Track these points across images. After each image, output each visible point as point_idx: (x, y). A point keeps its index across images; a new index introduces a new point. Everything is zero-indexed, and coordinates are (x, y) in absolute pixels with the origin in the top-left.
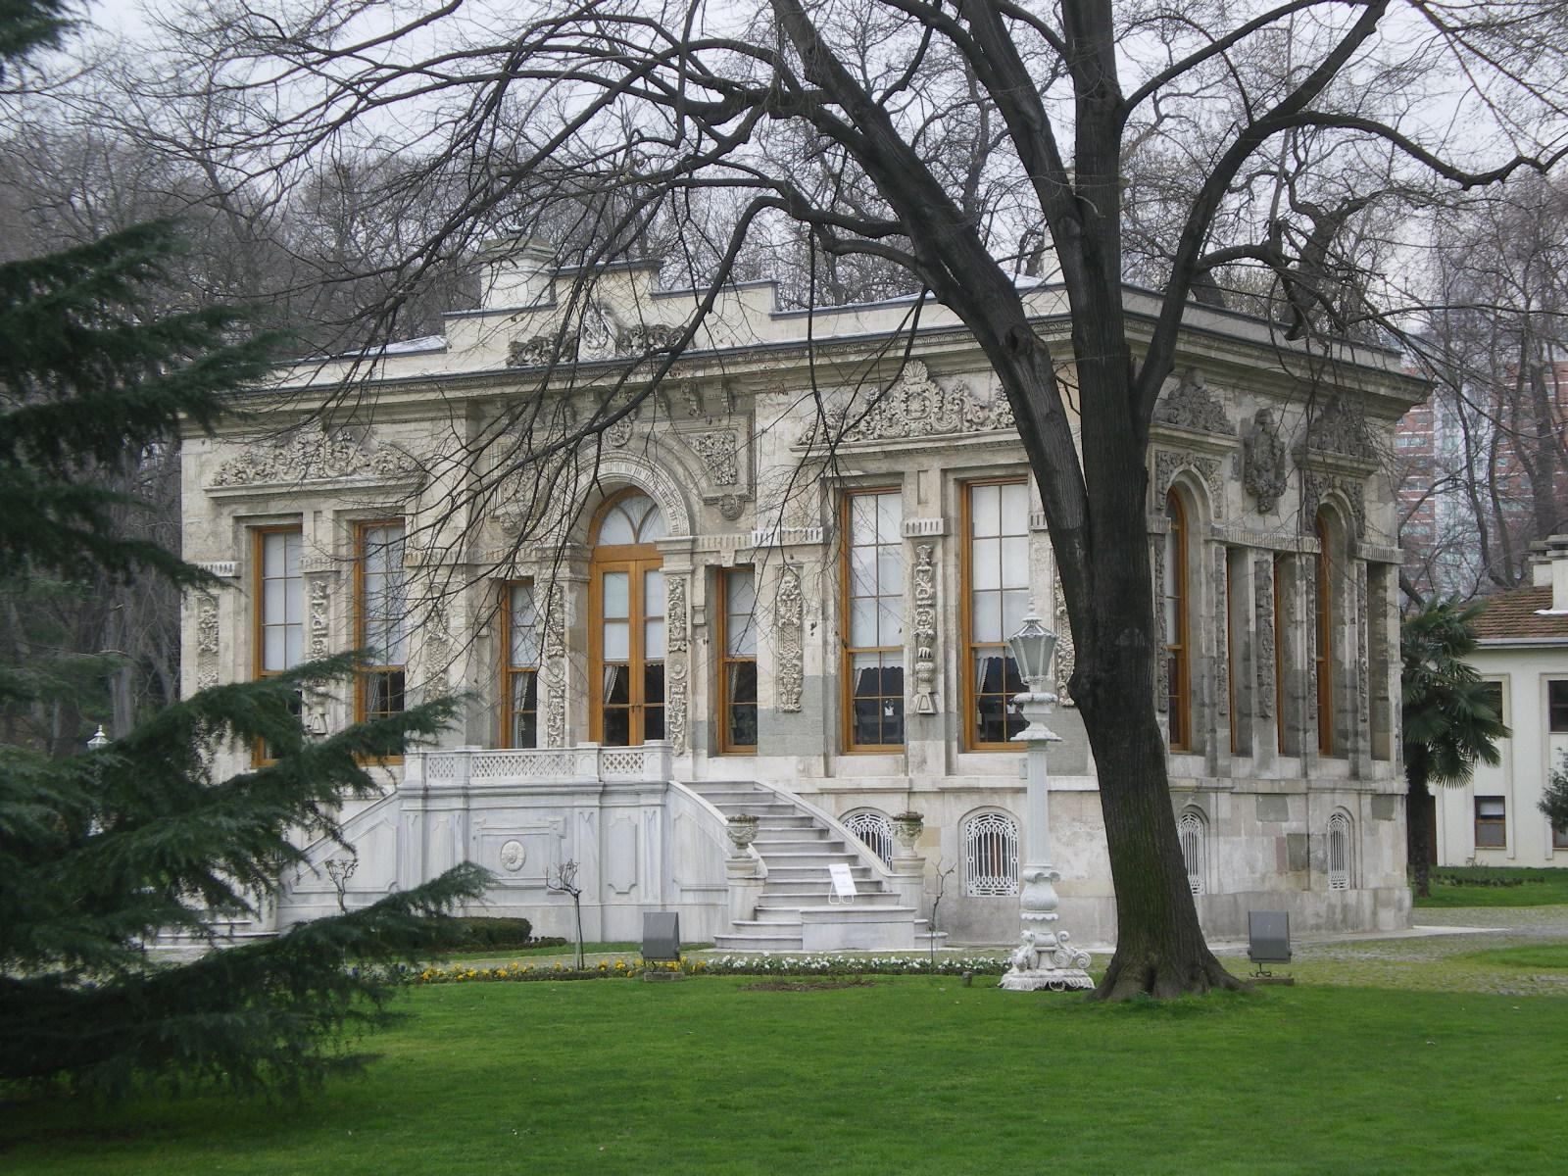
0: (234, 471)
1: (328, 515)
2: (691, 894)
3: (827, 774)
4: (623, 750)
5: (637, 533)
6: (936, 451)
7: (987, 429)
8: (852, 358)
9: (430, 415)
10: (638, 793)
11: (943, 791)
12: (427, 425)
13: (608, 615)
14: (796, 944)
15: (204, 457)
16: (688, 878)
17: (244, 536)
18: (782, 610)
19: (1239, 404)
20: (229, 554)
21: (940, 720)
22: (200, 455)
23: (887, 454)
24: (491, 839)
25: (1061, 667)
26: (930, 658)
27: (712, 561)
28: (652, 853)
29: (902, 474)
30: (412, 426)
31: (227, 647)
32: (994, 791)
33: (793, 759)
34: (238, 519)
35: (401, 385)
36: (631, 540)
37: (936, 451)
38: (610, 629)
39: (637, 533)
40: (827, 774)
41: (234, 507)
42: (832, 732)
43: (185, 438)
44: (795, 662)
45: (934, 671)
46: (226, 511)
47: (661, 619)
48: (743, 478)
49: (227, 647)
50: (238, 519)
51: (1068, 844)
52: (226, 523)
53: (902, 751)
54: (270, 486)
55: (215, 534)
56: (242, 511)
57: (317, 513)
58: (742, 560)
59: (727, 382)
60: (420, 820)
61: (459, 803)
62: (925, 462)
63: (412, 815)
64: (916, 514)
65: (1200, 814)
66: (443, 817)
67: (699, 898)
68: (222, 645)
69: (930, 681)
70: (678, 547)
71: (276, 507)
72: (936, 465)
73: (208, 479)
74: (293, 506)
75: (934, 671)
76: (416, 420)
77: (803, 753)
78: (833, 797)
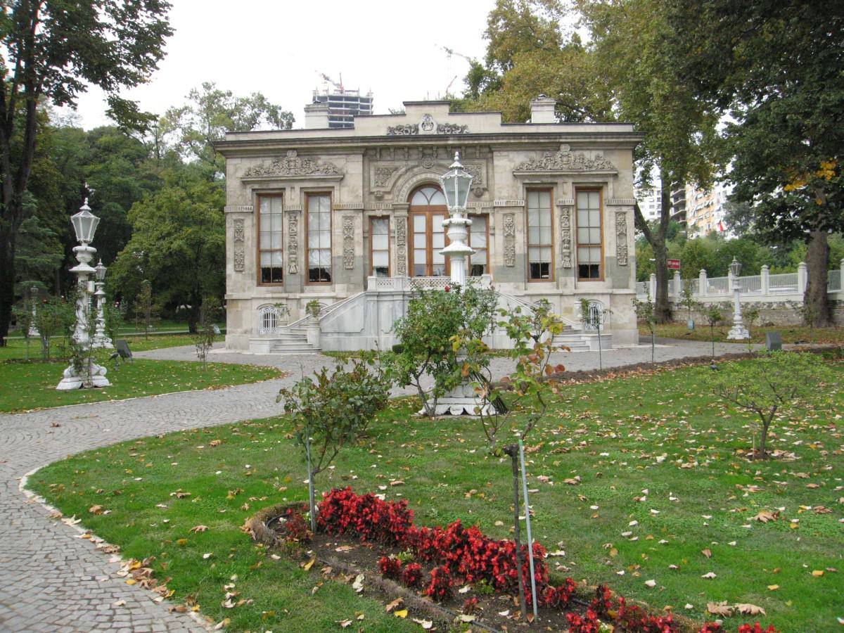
3: (526, 289)
5: (429, 202)
6: (572, 176)
7: (594, 169)
10: (393, 295)
12: (344, 156)
13: (415, 231)
17: (255, 197)
18: (507, 229)
19: (149, 142)
20: (250, 203)
21: (573, 270)
23: (552, 176)
26: (569, 248)
29: (556, 183)
31: (248, 239)
32: (595, 294)
33: (512, 284)
34: (253, 190)
36: (426, 203)
37: (572, 176)
39: (429, 202)
40: (526, 289)
45: (570, 253)
46: (248, 186)
48: (484, 182)
49: (248, 239)
50: (253, 190)
51: (622, 312)
52: (249, 191)
53: (282, 286)
55: (242, 195)
56: (256, 187)
57: (292, 188)
58: (485, 212)
59: (488, 146)
60: (376, 305)
61: (375, 298)
62: (566, 179)
63: (372, 303)
64: (562, 197)
65: (14, 323)
66: (386, 304)
68: (246, 238)
69: (569, 256)
72: (570, 181)
73: (241, 174)
74: (280, 185)
75: (570, 253)
77: (516, 281)
78: (529, 298)
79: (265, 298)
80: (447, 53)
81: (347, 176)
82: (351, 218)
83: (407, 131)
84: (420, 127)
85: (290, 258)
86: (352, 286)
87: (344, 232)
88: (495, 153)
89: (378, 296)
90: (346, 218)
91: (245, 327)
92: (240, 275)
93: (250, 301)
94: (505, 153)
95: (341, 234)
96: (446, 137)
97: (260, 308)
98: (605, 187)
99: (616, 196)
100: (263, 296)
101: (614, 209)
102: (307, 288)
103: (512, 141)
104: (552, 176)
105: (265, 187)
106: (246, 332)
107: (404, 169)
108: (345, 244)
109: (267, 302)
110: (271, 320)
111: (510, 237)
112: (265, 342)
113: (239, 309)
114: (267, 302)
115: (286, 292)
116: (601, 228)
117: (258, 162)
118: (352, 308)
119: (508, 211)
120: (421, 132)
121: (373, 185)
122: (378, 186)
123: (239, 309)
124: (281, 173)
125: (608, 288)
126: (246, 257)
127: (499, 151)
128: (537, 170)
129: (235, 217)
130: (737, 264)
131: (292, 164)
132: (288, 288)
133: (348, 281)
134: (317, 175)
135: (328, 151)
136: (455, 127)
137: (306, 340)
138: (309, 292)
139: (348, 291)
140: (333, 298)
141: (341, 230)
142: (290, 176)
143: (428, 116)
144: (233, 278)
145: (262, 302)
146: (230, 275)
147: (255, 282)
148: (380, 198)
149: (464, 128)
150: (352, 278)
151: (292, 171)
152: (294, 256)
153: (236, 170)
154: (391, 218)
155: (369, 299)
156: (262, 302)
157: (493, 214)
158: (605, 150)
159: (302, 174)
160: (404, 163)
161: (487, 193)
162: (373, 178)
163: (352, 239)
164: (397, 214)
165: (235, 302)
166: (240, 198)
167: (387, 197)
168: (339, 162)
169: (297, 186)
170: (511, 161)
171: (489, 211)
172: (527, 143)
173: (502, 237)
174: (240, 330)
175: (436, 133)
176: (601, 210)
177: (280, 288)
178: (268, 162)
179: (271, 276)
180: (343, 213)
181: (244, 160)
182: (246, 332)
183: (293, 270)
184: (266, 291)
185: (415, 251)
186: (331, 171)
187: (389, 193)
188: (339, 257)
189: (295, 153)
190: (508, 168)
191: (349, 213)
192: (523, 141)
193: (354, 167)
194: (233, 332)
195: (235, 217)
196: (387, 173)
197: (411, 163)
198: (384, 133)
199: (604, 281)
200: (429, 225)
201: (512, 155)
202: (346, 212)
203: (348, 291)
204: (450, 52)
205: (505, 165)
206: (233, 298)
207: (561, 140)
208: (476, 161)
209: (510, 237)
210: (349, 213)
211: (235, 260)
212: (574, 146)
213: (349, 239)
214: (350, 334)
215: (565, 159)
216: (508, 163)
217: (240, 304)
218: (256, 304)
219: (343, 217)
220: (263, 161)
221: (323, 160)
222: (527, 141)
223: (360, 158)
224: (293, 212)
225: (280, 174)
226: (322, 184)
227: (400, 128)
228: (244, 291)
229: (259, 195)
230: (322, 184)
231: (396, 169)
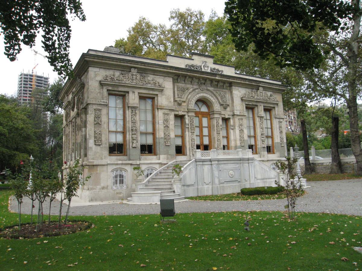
0: (110, 78)
1: (136, 94)
2: (259, 180)
4: (207, 151)
8: (253, 84)
9: (164, 75)
11: (268, 161)
14: (171, 186)
15: (97, 73)
16: (259, 177)
22: (95, 72)
24: (226, 170)
25: (96, 136)
27: (223, 116)
28: (251, 170)
30: (159, 77)
34: (108, 90)
35: (163, 67)
37: (263, 102)
38: (207, 126)
39: (200, 109)
41: (108, 87)
42: (158, 147)
43: (90, 66)
44: (100, 133)
46: (105, 87)
47: (196, 127)
49: (104, 123)
52: (105, 90)
54: (122, 83)
56: (110, 88)
58: (229, 117)
61: (210, 163)
63: (200, 166)
67: (261, 181)
68: (103, 122)
70: (218, 112)
71: (121, 89)
72: (262, 105)
73: (99, 78)
76: (160, 76)
79: (117, 164)
80: (34, 53)
81: (165, 89)
82: (167, 114)
83: (196, 68)
84: (202, 67)
85: (132, 137)
86: (169, 156)
87: (164, 123)
88: (233, 87)
89: (218, 161)
90: (165, 114)
91: (102, 185)
92: (99, 148)
93: (105, 167)
94: (237, 88)
95: (162, 124)
96: (215, 75)
97: (113, 171)
98: (273, 109)
99: (235, 116)
100: (116, 162)
101: (278, 120)
102: (143, 157)
103: (242, 82)
104: (257, 102)
105: (115, 89)
106: (103, 188)
107: (191, 90)
108: (165, 130)
109: (118, 166)
110: (118, 179)
111: (241, 131)
112: (156, 195)
113: (98, 172)
114: (118, 166)
115: (130, 160)
116: (272, 128)
117: (109, 73)
118: (190, 169)
119: (240, 117)
120: (203, 70)
121: (176, 96)
122: (179, 97)
123: (98, 172)
124: (128, 82)
125: (278, 157)
126: (103, 135)
127: (235, 86)
128: (251, 98)
129: (95, 107)
130: (32, 158)
131: (134, 77)
132: (131, 157)
133: (167, 153)
134: (149, 86)
135: (155, 72)
136: (218, 70)
137: (174, 192)
138: (143, 160)
139: (167, 159)
140: (159, 164)
141: (162, 121)
142: (134, 83)
143: (206, 62)
144: (93, 149)
145: (115, 167)
146: (91, 148)
147: (108, 152)
148: (180, 105)
149: (222, 71)
150: (169, 151)
151: (134, 81)
152: (135, 136)
153: (96, 75)
154: (186, 117)
155: (198, 163)
156: (115, 167)
157: (233, 118)
158: (273, 92)
159: (140, 84)
160: (192, 86)
161: (228, 107)
162: (176, 92)
163: (168, 127)
164: (190, 114)
165: (95, 167)
166: (99, 94)
167: (183, 104)
168: (160, 80)
169: (137, 91)
170: (239, 92)
171: (231, 117)
172: (254, 85)
173: (238, 131)
174: (98, 187)
175: (210, 72)
176: (271, 120)
177: (125, 157)
178: (117, 73)
179: (117, 149)
180: (163, 111)
181: (101, 69)
182: (103, 188)
183: (134, 145)
184: (114, 159)
185: (207, 135)
186: (157, 84)
187: (184, 102)
188: (162, 138)
189: (136, 70)
190: (239, 95)
191: (166, 112)
192: (246, 83)
193: (168, 84)
194: (94, 189)
195: (95, 107)
196: (183, 90)
197: (195, 87)
198: (183, 66)
199: (274, 153)
200: (201, 122)
201: (240, 89)
202: (165, 110)
203: (167, 159)
204: (36, 52)
205: (238, 93)
206: (94, 164)
207: (261, 85)
208: (224, 90)
209: (241, 131)
210: (166, 112)
211: (95, 137)
212: (265, 88)
213: (167, 127)
214: (188, 186)
215: (261, 94)
216: (239, 93)
217: (99, 168)
218: (110, 168)
219: (164, 113)
220: (114, 72)
221: (150, 77)
222: (248, 83)
223: (171, 79)
224: (134, 107)
225: (127, 82)
226: (151, 92)
227: (193, 66)
228: (102, 159)
229: (109, 94)
230: (151, 92)
231: (187, 89)
